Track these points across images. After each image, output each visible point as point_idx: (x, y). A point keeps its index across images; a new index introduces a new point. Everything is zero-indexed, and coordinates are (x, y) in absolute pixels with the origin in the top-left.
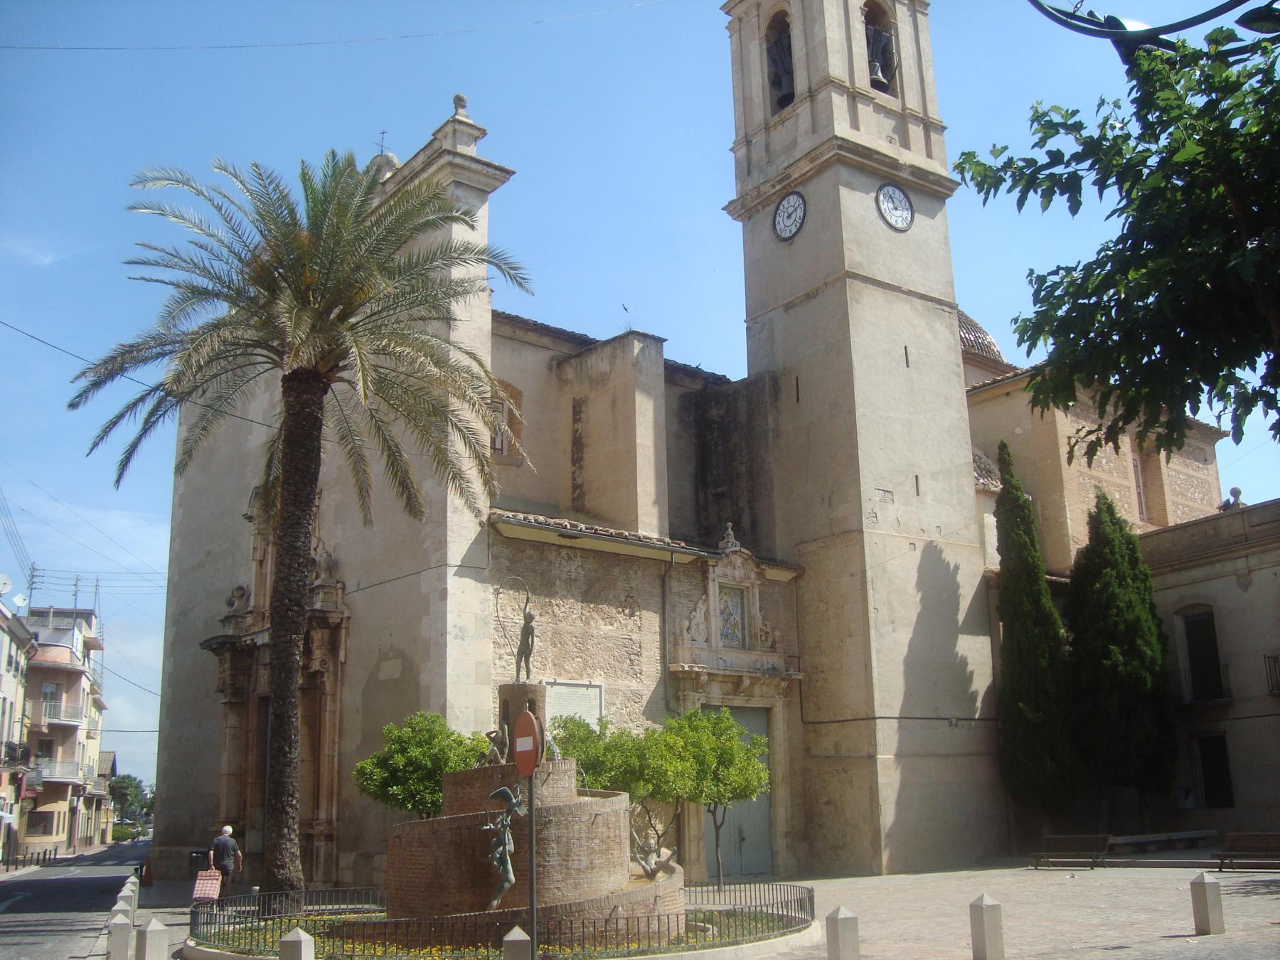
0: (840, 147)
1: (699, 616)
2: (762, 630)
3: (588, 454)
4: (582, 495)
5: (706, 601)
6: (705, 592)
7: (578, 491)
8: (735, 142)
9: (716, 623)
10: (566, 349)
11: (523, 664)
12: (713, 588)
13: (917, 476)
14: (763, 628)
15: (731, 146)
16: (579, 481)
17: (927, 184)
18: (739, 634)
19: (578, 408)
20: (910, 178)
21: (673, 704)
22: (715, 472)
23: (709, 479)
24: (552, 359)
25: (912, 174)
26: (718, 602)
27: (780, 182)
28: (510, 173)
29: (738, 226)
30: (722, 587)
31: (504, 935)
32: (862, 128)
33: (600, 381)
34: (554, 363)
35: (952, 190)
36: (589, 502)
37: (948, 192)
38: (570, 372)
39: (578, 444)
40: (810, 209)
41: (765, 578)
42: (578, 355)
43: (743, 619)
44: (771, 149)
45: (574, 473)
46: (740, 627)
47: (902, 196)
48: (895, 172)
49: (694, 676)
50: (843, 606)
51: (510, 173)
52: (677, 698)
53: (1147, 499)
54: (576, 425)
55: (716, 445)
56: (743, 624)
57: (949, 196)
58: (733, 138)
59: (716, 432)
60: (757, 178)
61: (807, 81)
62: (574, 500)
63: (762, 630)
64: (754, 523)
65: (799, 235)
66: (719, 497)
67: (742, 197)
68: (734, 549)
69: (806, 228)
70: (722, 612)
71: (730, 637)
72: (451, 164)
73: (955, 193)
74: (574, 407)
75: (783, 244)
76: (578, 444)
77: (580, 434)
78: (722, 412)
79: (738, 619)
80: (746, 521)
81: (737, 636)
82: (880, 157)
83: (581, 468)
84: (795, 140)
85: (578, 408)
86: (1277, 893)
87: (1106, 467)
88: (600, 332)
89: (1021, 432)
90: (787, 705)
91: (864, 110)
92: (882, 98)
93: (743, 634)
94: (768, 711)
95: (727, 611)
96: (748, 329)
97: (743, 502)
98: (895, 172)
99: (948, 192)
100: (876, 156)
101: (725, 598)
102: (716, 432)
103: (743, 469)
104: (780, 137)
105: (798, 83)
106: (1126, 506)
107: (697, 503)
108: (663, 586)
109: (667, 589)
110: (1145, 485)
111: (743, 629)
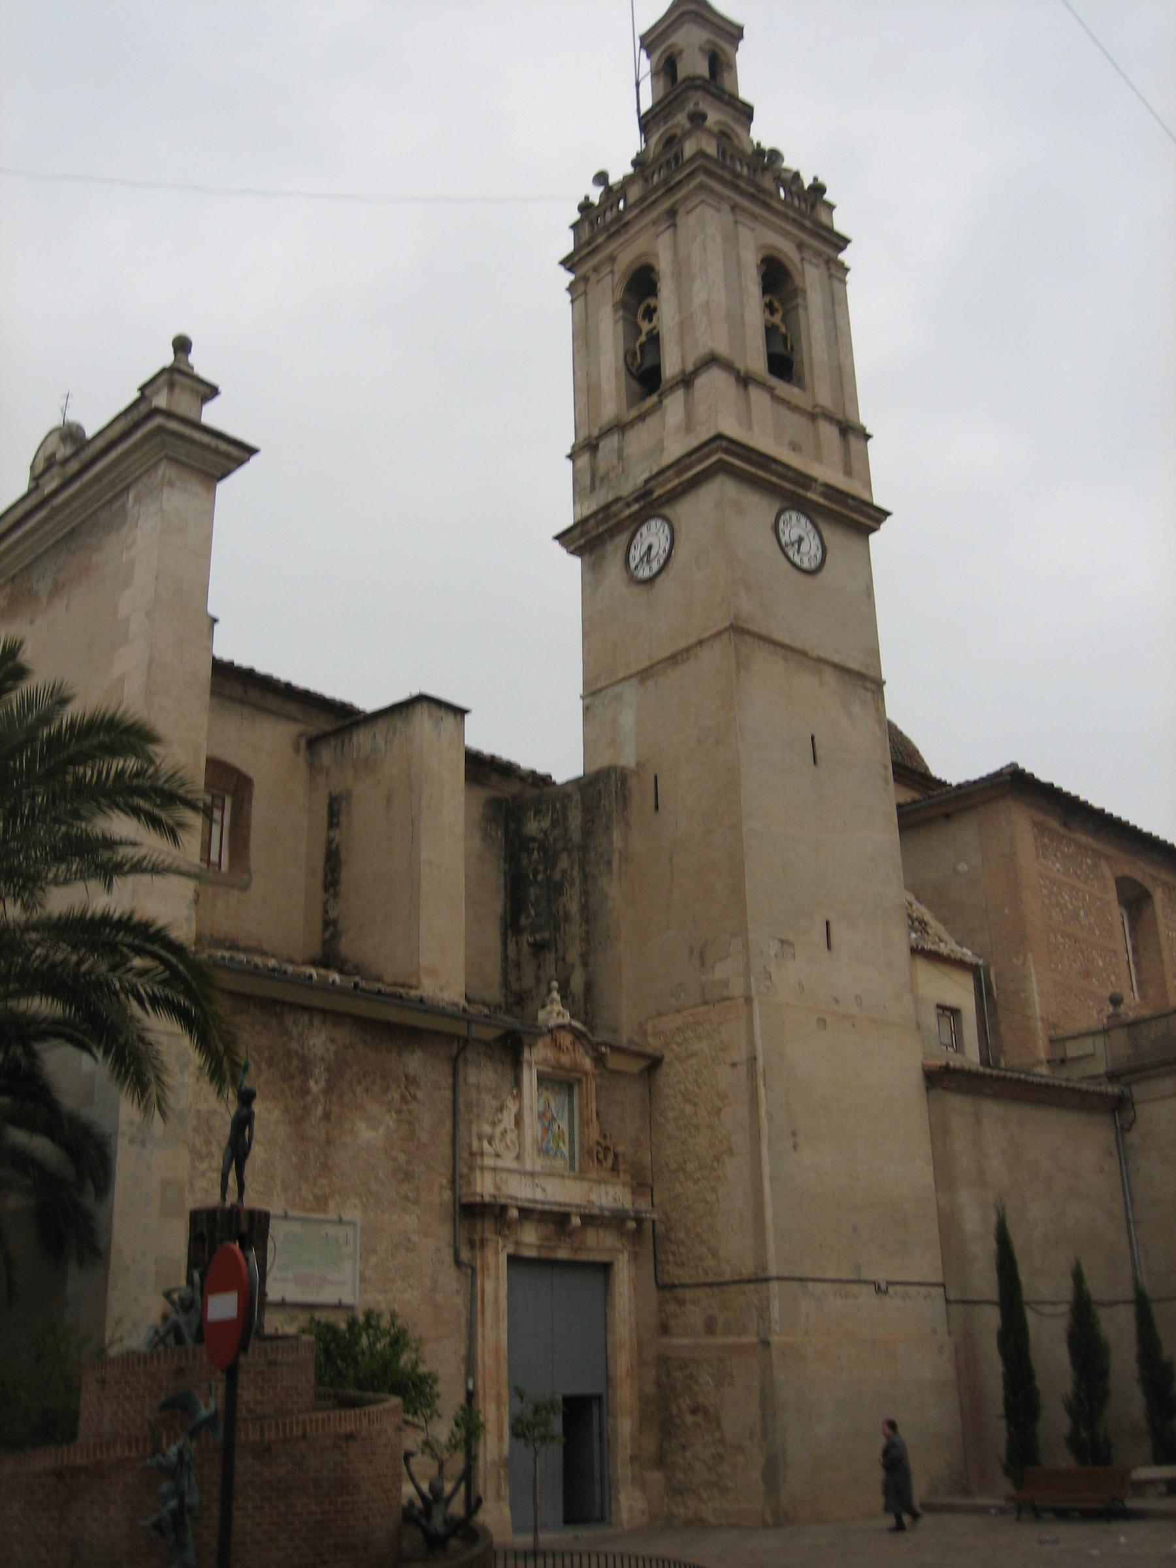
0: (727, 451)
1: (508, 1121)
2: (598, 1143)
3: (348, 874)
4: (335, 937)
5: (519, 1096)
6: (517, 1082)
7: (331, 929)
8: (573, 447)
9: (532, 1129)
10: (324, 724)
11: (232, 1175)
12: (529, 1078)
13: (827, 923)
14: (602, 1141)
15: (569, 451)
16: (333, 914)
17: (845, 511)
18: (565, 1149)
19: (335, 810)
20: (821, 500)
21: (465, 1255)
22: (532, 912)
23: (524, 921)
24: (300, 735)
25: (824, 495)
26: (535, 1099)
27: (636, 500)
28: (251, 451)
29: (575, 563)
30: (542, 1079)
31: (803, 187)
32: (756, 428)
33: (368, 765)
34: (303, 742)
35: (879, 522)
36: (345, 947)
37: (870, 523)
38: (326, 755)
39: (333, 860)
40: (681, 539)
41: (605, 1066)
42: (338, 732)
43: (571, 1126)
44: (625, 454)
45: (326, 903)
46: (567, 1139)
47: (809, 526)
48: (801, 491)
49: (497, 1211)
50: (720, 1109)
51: (251, 451)
52: (472, 1244)
53: (1138, 971)
54: (332, 834)
55: (536, 873)
56: (571, 1135)
57: (874, 530)
58: (571, 440)
59: (536, 853)
60: (603, 496)
61: (680, 360)
62: (325, 942)
63: (598, 1143)
64: (589, 987)
65: (663, 575)
66: (539, 948)
67: (581, 524)
68: (560, 1021)
69: (676, 563)
70: (541, 1116)
71: (552, 1153)
72: (160, 429)
73: (883, 526)
74: (331, 806)
75: (637, 590)
76: (333, 860)
77: (337, 846)
78: (546, 824)
79: (564, 1126)
80: (577, 983)
81: (562, 1153)
82: (780, 469)
83: (336, 895)
84: (661, 441)
85: (335, 810)
86: (1166, 1516)
87: (1085, 923)
88: (368, 703)
89: (966, 868)
90: (635, 1257)
91: (758, 396)
92: (783, 388)
93: (572, 1150)
94: (606, 1268)
95: (548, 1115)
96: (586, 709)
97: (573, 956)
98: (801, 491)
99: (870, 523)
100: (774, 466)
101: (546, 1094)
102: (536, 853)
103: (574, 908)
104: (639, 439)
105: (667, 365)
106: (1113, 978)
107: (505, 957)
108: (455, 1074)
109: (461, 1078)
110: (1135, 951)
111: (572, 1142)
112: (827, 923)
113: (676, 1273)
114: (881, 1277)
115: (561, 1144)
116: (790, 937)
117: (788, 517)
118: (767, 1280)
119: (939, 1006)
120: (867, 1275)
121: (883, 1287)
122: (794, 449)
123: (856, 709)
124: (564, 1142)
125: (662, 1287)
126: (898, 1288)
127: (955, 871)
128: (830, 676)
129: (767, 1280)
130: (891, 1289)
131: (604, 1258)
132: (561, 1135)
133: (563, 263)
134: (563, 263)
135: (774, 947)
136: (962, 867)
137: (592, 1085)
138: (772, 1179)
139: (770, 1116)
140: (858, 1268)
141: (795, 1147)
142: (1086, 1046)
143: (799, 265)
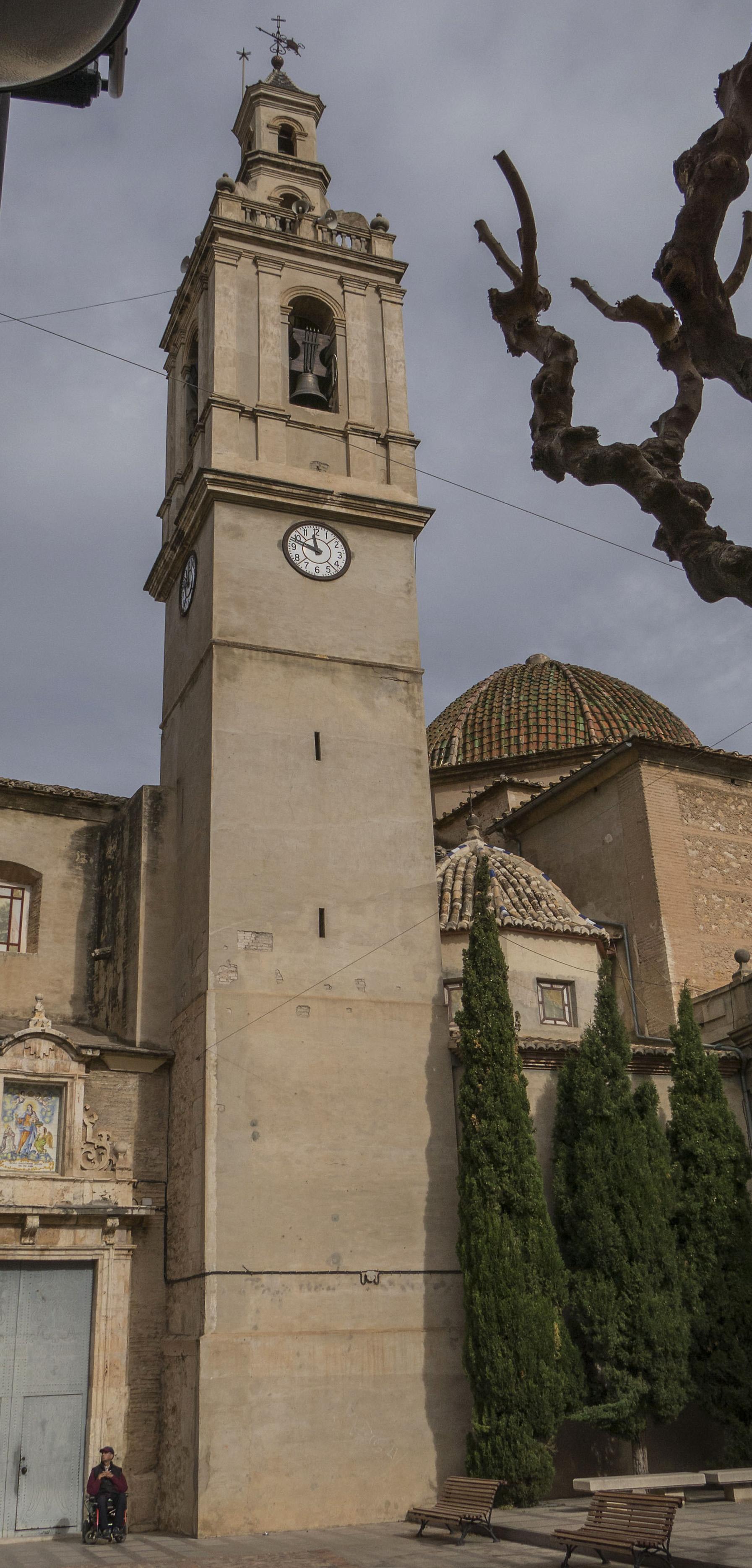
13: (322, 912)
47: (331, 536)
81: (47, 1155)
112: (322, 912)
113: (176, 1271)
114: (369, 1266)
115: (46, 1147)
116: (268, 928)
117: (302, 532)
118: (424, 1272)
119: (539, 981)
120: (347, 1264)
121: (371, 1276)
122: (318, 469)
123: (382, 700)
124: (51, 1146)
125: (169, 1283)
126: (389, 1277)
127: (604, 843)
128: (347, 674)
129: (424, 1272)
130: (384, 1279)
131: (87, 1257)
132: (47, 1139)
133: (160, 346)
134: (160, 346)
135: (244, 939)
136: (609, 838)
137: (78, 1090)
138: (219, 1171)
139: (222, 1108)
140: (337, 1258)
141: (255, 1137)
142: (718, 1008)
143: (340, 300)
